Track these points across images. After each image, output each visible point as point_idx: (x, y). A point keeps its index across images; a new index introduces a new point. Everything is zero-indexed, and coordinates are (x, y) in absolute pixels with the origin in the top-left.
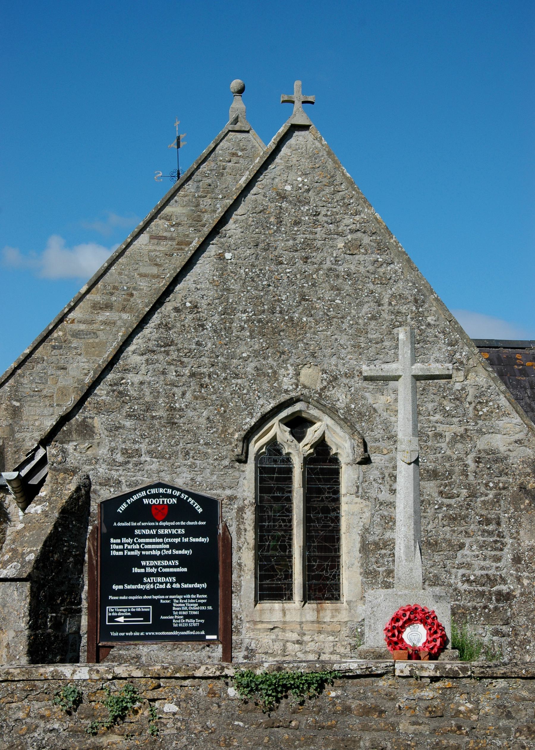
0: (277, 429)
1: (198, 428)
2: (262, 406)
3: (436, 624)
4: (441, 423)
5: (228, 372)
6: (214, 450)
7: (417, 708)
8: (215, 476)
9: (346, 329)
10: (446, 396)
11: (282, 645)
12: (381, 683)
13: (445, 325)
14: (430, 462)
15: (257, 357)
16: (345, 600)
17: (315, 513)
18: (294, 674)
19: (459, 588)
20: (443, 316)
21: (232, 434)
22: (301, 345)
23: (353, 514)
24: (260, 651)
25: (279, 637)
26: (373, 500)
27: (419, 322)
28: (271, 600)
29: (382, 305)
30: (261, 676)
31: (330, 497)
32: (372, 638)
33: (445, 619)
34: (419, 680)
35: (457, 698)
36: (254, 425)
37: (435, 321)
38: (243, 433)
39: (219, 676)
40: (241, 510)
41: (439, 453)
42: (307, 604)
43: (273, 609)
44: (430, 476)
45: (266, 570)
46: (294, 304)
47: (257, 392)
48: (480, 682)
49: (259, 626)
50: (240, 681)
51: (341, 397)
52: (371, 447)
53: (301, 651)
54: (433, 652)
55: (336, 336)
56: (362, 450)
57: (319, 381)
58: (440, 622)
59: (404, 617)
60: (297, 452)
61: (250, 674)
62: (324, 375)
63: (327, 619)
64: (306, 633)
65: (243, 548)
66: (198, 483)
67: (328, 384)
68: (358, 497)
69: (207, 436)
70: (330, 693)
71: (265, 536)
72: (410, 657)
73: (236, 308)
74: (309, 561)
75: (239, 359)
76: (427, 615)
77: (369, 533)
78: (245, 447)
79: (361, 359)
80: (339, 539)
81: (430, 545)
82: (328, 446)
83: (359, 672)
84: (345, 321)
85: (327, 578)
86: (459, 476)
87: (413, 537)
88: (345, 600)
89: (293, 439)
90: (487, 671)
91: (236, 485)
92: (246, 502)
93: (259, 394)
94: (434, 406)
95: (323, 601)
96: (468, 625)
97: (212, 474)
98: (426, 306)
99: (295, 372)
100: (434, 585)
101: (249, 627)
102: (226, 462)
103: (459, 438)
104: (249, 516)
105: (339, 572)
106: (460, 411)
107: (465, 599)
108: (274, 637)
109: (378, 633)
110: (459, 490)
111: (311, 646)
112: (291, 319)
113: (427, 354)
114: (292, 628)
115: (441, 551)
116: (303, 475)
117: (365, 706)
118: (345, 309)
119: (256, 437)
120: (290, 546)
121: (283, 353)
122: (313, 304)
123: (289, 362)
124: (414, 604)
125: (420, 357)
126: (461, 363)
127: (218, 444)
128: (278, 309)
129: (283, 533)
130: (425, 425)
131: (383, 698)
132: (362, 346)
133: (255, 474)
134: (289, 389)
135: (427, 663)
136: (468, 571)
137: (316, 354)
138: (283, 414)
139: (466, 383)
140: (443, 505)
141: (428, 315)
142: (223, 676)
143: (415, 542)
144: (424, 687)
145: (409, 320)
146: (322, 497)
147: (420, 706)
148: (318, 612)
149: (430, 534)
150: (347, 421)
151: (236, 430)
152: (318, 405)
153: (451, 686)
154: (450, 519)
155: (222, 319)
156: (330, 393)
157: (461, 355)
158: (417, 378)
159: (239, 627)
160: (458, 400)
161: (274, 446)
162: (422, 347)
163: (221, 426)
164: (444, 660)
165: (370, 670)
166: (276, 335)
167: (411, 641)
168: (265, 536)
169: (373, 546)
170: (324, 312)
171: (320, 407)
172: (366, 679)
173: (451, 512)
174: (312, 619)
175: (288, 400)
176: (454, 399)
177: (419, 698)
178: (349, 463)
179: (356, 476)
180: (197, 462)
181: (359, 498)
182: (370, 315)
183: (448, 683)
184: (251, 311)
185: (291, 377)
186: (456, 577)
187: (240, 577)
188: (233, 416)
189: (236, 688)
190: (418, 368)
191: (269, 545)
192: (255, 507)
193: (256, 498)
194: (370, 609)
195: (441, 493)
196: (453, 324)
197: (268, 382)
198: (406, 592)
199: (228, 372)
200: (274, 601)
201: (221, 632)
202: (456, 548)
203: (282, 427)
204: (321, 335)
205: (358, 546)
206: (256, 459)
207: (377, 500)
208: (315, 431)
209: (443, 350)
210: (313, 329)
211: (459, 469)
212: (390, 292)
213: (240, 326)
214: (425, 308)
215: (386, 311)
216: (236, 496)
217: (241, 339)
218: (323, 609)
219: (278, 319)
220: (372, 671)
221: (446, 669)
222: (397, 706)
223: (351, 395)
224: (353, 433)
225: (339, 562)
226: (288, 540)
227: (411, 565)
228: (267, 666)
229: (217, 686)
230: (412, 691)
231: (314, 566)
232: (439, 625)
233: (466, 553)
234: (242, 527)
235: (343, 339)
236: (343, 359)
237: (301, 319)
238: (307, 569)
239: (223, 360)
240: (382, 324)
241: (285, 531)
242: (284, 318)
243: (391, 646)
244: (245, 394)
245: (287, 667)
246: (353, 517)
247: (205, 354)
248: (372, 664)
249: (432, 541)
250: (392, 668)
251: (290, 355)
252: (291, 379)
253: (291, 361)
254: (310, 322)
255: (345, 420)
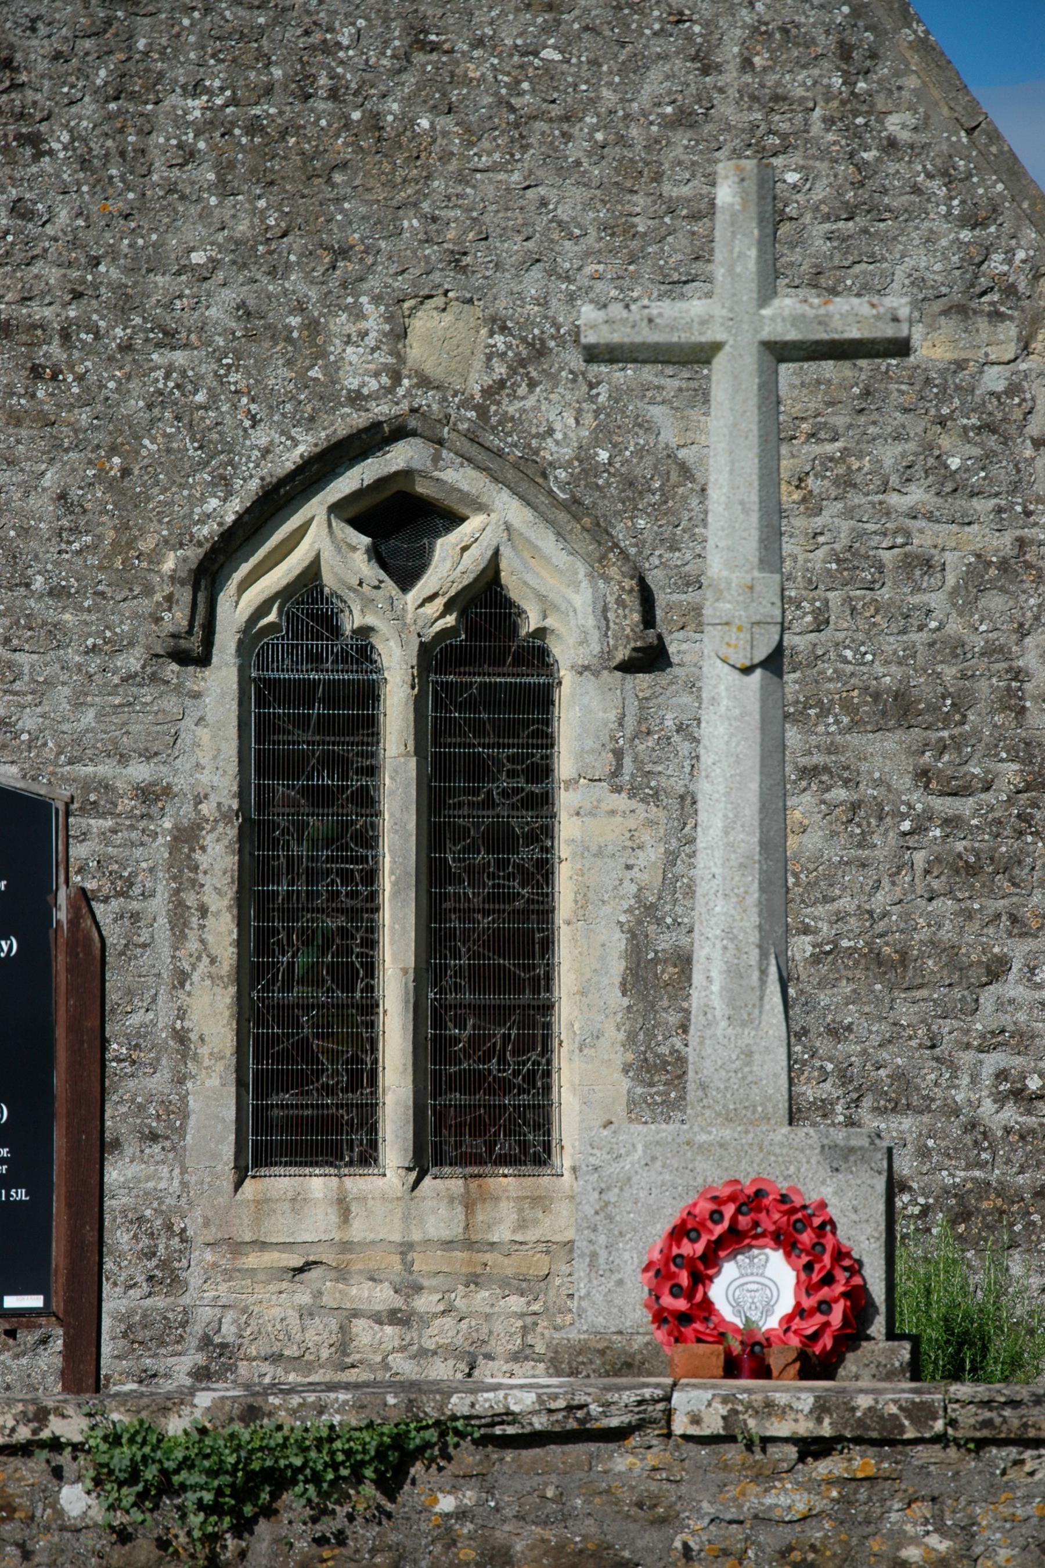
0: (321, 540)
1: (24, 532)
2: (266, 452)
3: (829, 1249)
4: (930, 517)
5: (138, 320)
6: (85, 616)
7: (750, 1553)
8: (91, 714)
9: (578, 163)
10: (951, 417)
11: (334, 1327)
12: (623, 1461)
13: (952, 145)
14: (887, 662)
15: (245, 266)
16: (567, 1163)
17: (464, 850)
18: (306, 1430)
19: (987, 1122)
20: (945, 111)
21: (155, 557)
22: (411, 223)
23: (599, 854)
24: (253, 1351)
25: (326, 1300)
26: (674, 803)
27: (854, 134)
28: (296, 1164)
29: (718, 68)
30: (182, 1439)
31: (517, 791)
32: (598, 1298)
33: (861, 1236)
34: (757, 1449)
35: (894, 1516)
36: (235, 522)
37: (916, 129)
38: (194, 554)
39: (30, 1443)
40: (187, 837)
41: (920, 629)
42: (427, 1181)
43: (306, 1200)
44: (884, 713)
45: (279, 1058)
46: (384, 62)
47: (245, 400)
48: (978, 1459)
49: (252, 1260)
50: (104, 1458)
51: (558, 420)
52: (670, 607)
53: (403, 1349)
54: (817, 1350)
55: (542, 191)
56: (636, 617)
57: (478, 363)
58: (844, 1242)
59: (716, 1223)
60: (397, 626)
61: (144, 1434)
62: (499, 340)
63: (502, 1233)
64: (425, 1283)
65: (196, 977)
66: (25, 737)
67: (513, 371)
68: (617, 790)
69: (57, 564)
70: (436, 1501)
71: (275, 932)
72: (732, 1368)
73: (161, 75)
74: (438, 1022)
75: (178, 273)
76: (799, 1215)
77: (659, 922)
78: (201, 608)
79: (635, 277)
80: (548, 944)
81: (880, 964)
82: (509, 603)
83: (539, 1423)
84: (575, 131)
85: (506, 1086)
86: (992, 712)
87: (754, 937)
88: (567, 1163)
89: (383, 575)
90: (1005, 1420)
91: (167, 746)
92: (204, 808)
93: (253, 407)
94: (903, 455)
95: (488, 1169)
96: (1016, 1254)
97: (78, 704)
98: (883, 71)
99: (387, 327)
100: (893, 1110)
101: (215, 1265)
102: (132, 661)
103: (993, 572)
104: (218, 858)
105: (549, 1062)
106: (1002, 472)
107: (1008, 1162)
108: (304, 1298)
109: (620, 1282)
110: (992, 766)
111: (442, 1332)
112: (375, 122)
113: (884, 259)
114: (372, 1265)
115: (920, 986)
116: (416, 710)
117: (560, 1548)
118: (575, 86)
119: (245, 568)
120: (371, 968)
121: (343, 252)
122: (457, 63)
123: (365, 286)
124: (753, 1176)
125: (857, 269)
126: (1010, 291)
127: (102, 594)
128: (323, 80)
129: (341, 921)
130: (871, 527)
131: (628, 1516)
132: (641, 229)
133: (240, 704)
134: (365, 391)
135: (787, 1390)
136: (1018, 1061)
137: (468, 260)
138: (346, 483)
139: (1023, 366)
140: (930, 819)
141: (890, 106)
142: (42, 1444)
143: (764, 955)
144: (775, 1474)
145: (817, 127)
146: (489, 793)
147: (759, 1544)
148: (469, 1206)
149: (881, 926)
150: (583, 511)
151: (166, 542)
152: (473, 450)
153: (871, 1471)
154: (957, 872)
155: (110, 117)
156: (518, 404)
157: (1010, 262)
158: (779, 352)
159: (176, 1264)
160: (994, 431)
161: (309, 603)
162: (865, 231)
163: (110, 524)
164: (857, 1378)
165: (580, 1414)
166: (316, 181)
167: (738, 1313)
168: (275, 932)
169: (671, 970)
170: (496, 94)
171: (481, 456)
172: (569, 1448)
173: (960, 846)
174: (446, 1234)
175: (360, 431)
176: (979, 430)
177: (756, 1517)
178: (586, 668)
179: (612, 715)
180: (21, 658)
181: (624, 795)
182: (669, 110)
183: (863, 1462)
184: (222, 89)
185: (373, 344)
186: (974, 1079)
187: (181, 1081)
188: (156, 490)
189: (90, 1485)
190: (789, 314)
191: (291, 965)
192: (240, 828)
193: (242, 794)
194: (596, 1195)
195: (923, 775)
196: (984, 139)
197: (289, 363)
198: (727, 1133)
199: (138, 320)
200: (307, 1170)
201: (59, 1284)
202: (977, 975)
203: (339, 534)
204: (487, 187)
205: (617, 967)
206: (243, 649)
207: (689, 801)
208: (465, 549)
209: (944, 242)
210: (454, 162)
211: (994, 689)
212: (746, 16)
213: (180, 146)
214: (879, 82)
215: (733, 93)
216: (169, 786)
217: (183, 197)
218: (486, 1197)
219: (323, 123)
220: (588, 1417)
221: (853, 1409)
222: (678, 1544)
223: (597, 413)
224: (603, 557)
225: (548, 1026)
226: (361, 946)
227: (747, 1036)
228: (208, 1404)
229: (19, 1480)
230: (732, 1491)
231: (456, 1040)
232: (840, 1254)
233: (1012, 994)
234: (190, 899)
235: (570, 203)
236: (568, 279)
237: (413, 122)
238: (432, 1050)
239: (115, 274)
240: (715, 145)
241: (353, 914)
242: (347, 117)
243: (665, 1327)
244: (200, 407)
245: (278, 1408)
246: (599, 862)
247: (45, 250)
248: (588, 1394)
249: (887, 950)
250: (660, 1406)
251: (370, 260)
252: (373, 350)
253: (373, 283)
254: (445, 134)
255: (574, 507)
